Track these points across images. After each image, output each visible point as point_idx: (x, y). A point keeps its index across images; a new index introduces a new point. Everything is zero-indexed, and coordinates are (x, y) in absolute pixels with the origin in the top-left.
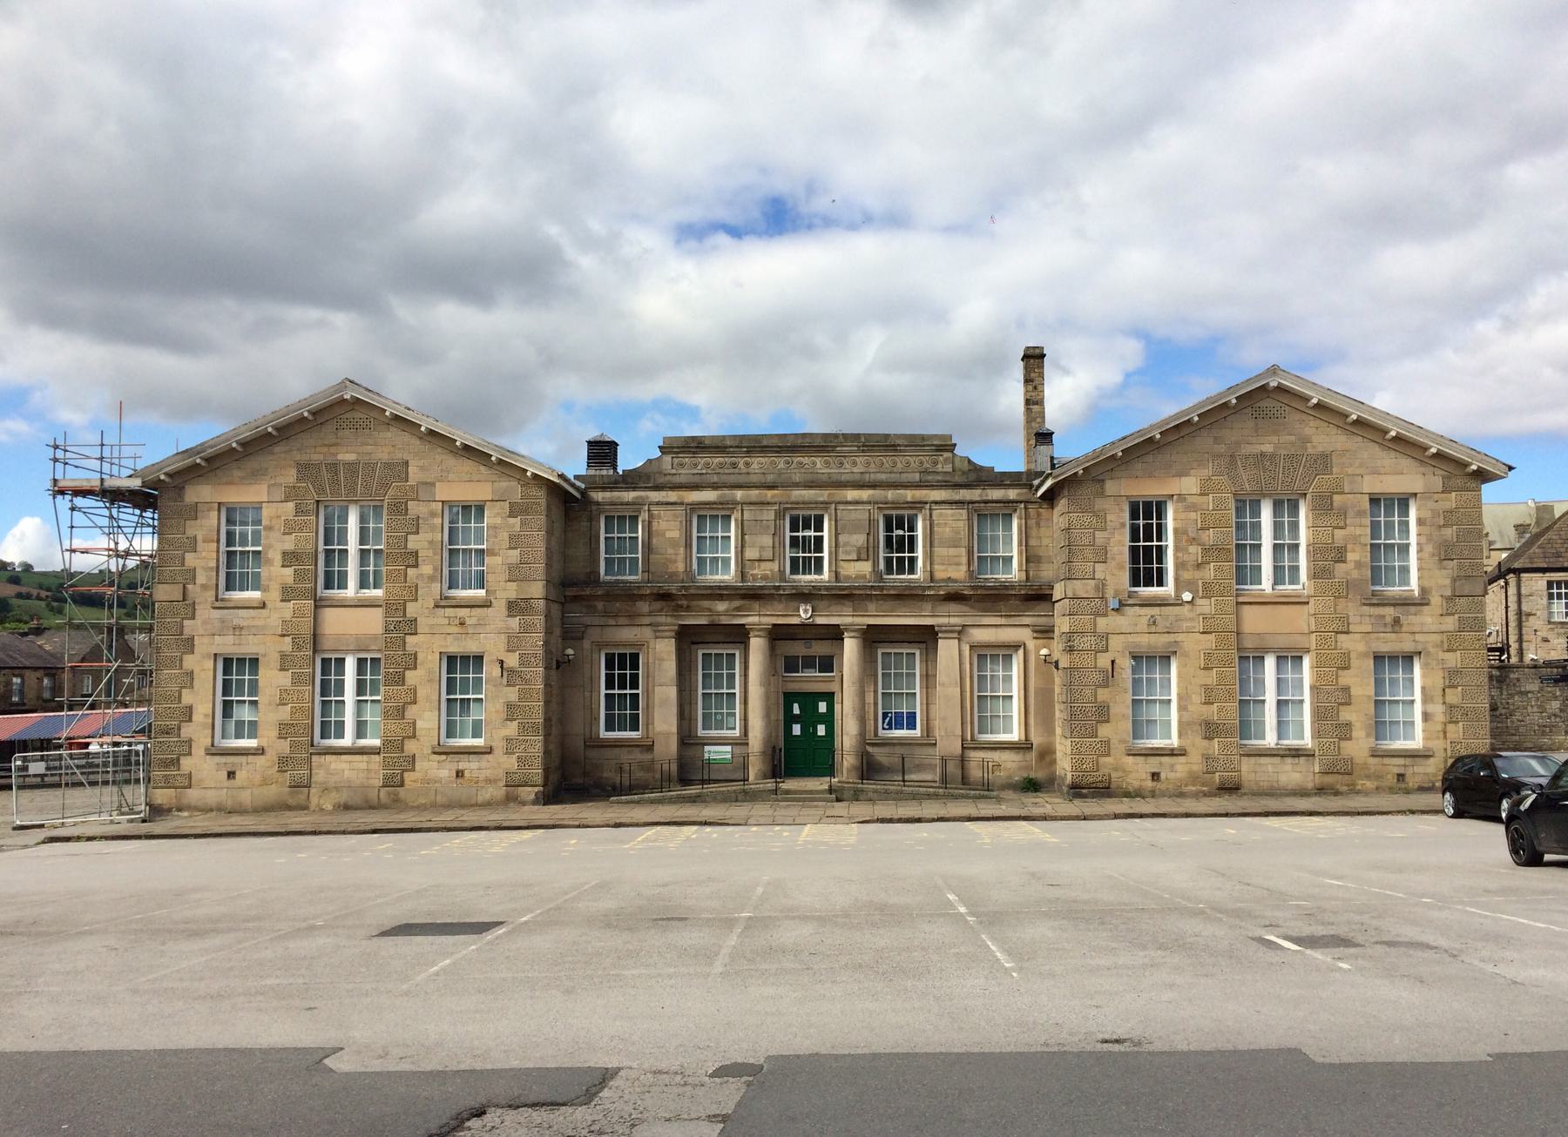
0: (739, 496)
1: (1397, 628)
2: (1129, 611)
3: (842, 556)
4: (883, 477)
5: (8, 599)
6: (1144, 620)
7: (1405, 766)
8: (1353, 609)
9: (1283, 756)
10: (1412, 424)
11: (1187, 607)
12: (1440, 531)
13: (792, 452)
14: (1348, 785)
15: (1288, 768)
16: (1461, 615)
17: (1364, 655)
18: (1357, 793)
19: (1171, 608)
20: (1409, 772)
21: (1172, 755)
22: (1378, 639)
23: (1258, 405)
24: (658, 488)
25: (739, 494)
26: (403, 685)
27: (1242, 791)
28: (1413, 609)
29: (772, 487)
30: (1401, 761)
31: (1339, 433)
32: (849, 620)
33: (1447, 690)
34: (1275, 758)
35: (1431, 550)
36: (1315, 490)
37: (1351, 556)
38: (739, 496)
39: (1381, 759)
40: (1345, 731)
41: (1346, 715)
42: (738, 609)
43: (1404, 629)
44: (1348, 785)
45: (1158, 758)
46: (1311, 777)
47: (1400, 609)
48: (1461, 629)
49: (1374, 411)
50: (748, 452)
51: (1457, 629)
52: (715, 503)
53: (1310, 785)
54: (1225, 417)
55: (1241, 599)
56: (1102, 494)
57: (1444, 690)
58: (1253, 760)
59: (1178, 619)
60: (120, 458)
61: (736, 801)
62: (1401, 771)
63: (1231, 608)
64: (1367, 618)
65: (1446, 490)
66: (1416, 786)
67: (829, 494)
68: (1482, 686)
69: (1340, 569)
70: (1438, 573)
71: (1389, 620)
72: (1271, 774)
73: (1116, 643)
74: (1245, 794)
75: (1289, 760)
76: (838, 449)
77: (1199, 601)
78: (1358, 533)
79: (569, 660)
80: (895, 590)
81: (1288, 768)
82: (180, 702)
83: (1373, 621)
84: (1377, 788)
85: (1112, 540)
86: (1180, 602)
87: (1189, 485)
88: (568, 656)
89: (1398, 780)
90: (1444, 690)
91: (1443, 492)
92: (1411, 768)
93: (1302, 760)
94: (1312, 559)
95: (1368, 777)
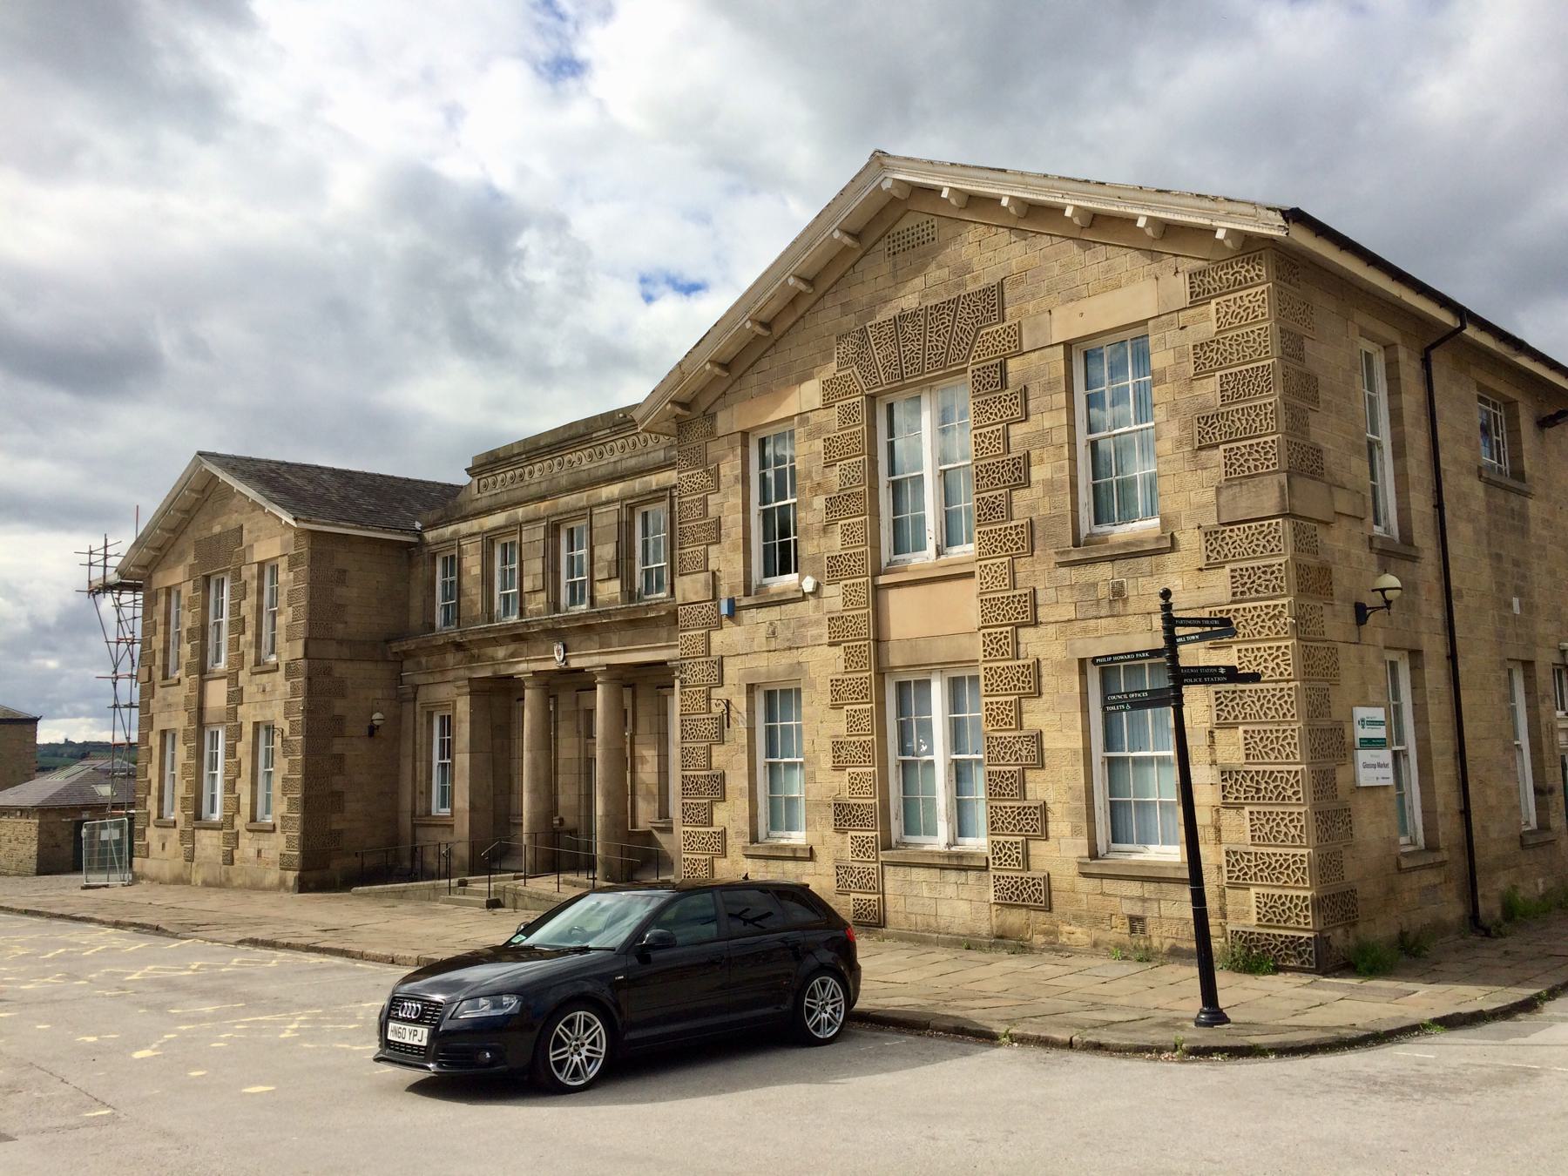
0: (520, 514)
1: (1119, 607)
2: (747, 616)
3: (597, 577)
4: (632, 462)
5: (922, 643)
6: (763, 631)
7: (1143, 900)
8: (1038, 573)
9: (943, 868)
10: (1087, 181)
11: (812, 601)
12: (1191, 389)
13: (561, 449)
14: (1046, 933)
15: (950, 890)
16: (1234, 566)
17: (1061, 667)
18: (1057, 951)
19: (791, 606)
20: (1151, 912)
21: (795, 859)
22: (1085, 630)
23: (895, 230)
24: (465, 519)
25: (520, 512)
26: (235, 757)
27: (889, 930)
28: (1145, 562)
29: (542, 498)
30: (1134, 889)
31: (1014, 239)
32: (596, 660)
33: (1217, 733)
34: (932, 871)
35: (1176, 433)
36: (977, 359)
37: (1037, 473)
38: (520, 514)
39: (1097, 881)
40: (1037, 821)
41: (1040, 788)
42: (512, 655)
43: (1130, 610)
44: (1046, 933)
45: (780, 863)
46: (985, 914)
47: (1121, 565)
48: (1239, 597)
49: (858, 184)
50: (528, 459)
51: (1230, 598)
52: (505, 527)
53: (984, 928)
54: (853, 266)
55: (882, 580)
56: (712, 434)
57: (1211, 732)
58: (901, 870)
59: (803, 624)
60: (91, 564)
61: (429, 899)
62: (1137, 910)
63: (865, 594)
64: (1067, 592)
65: (1198, 298)
66: (1166, 947)
67: (588, 496)
68: (1289, 723)
69: (1021, 498)
70: (1191, 479)
71: (1104, 591)
72: (927, 901)
73: (732, 670)
74: (888, 937)
75: (952, 876)
76: (594, 435)
77: (827, 591)
78: (1047, 425)
79: (1388, 603)
80: (621, 614)
81: (950, 890)
82: (1020, 727)
83: (1077, 596)
84: (1095, 945)
85: (726, 505)
86: (801, 595)
87: (808, 395)
88: (1383, 591)
89: (1133, 930)
90: (1211, 732)
91: (1193, 304)
92: (1156, 905)
93: (972, 875)
94: (976, 490)
95: (1078, 918)
